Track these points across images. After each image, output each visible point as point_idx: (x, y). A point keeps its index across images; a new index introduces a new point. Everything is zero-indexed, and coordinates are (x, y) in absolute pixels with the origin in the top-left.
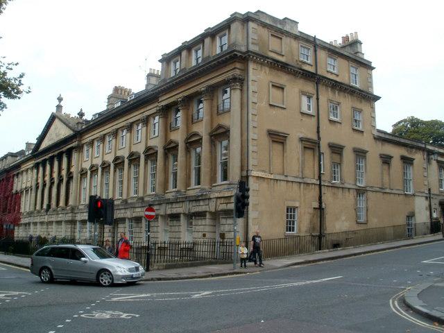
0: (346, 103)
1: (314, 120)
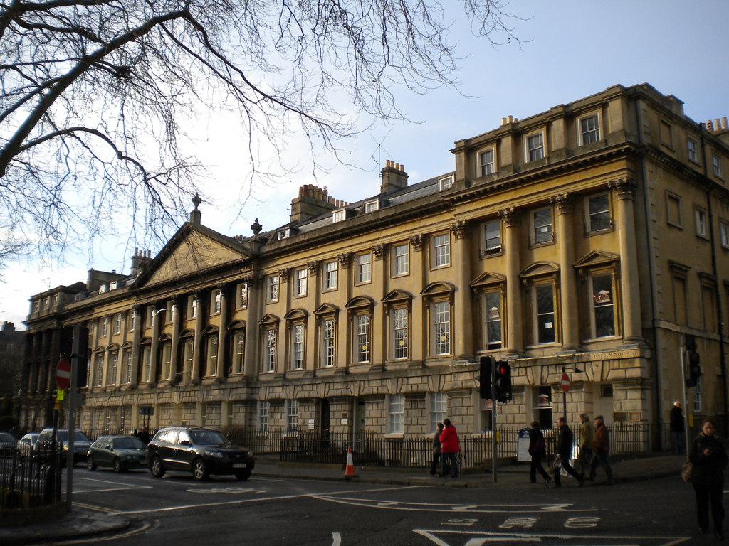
1: (708, 246)
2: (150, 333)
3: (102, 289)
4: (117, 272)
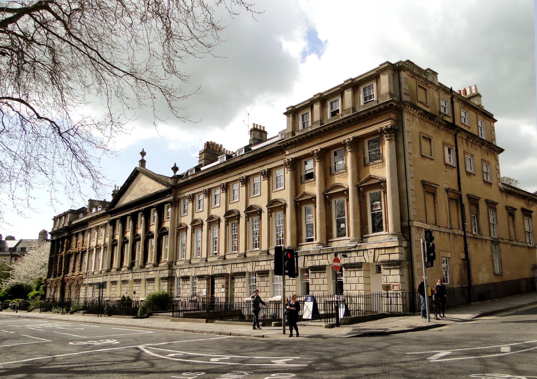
0: (478, 154)
1: (455, 171)
2: (118, 237)
3: (94, 210)
4: (107, 201)
